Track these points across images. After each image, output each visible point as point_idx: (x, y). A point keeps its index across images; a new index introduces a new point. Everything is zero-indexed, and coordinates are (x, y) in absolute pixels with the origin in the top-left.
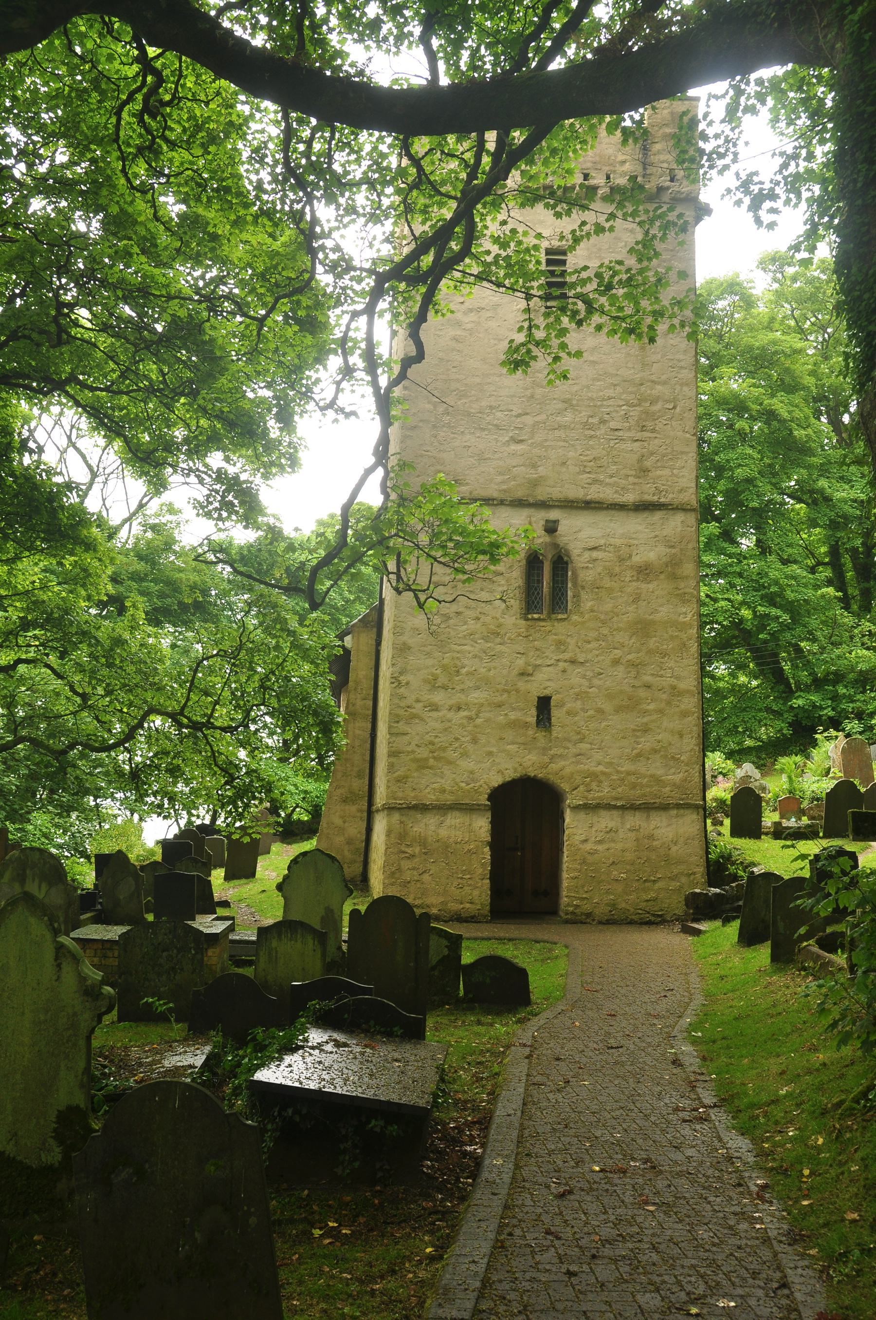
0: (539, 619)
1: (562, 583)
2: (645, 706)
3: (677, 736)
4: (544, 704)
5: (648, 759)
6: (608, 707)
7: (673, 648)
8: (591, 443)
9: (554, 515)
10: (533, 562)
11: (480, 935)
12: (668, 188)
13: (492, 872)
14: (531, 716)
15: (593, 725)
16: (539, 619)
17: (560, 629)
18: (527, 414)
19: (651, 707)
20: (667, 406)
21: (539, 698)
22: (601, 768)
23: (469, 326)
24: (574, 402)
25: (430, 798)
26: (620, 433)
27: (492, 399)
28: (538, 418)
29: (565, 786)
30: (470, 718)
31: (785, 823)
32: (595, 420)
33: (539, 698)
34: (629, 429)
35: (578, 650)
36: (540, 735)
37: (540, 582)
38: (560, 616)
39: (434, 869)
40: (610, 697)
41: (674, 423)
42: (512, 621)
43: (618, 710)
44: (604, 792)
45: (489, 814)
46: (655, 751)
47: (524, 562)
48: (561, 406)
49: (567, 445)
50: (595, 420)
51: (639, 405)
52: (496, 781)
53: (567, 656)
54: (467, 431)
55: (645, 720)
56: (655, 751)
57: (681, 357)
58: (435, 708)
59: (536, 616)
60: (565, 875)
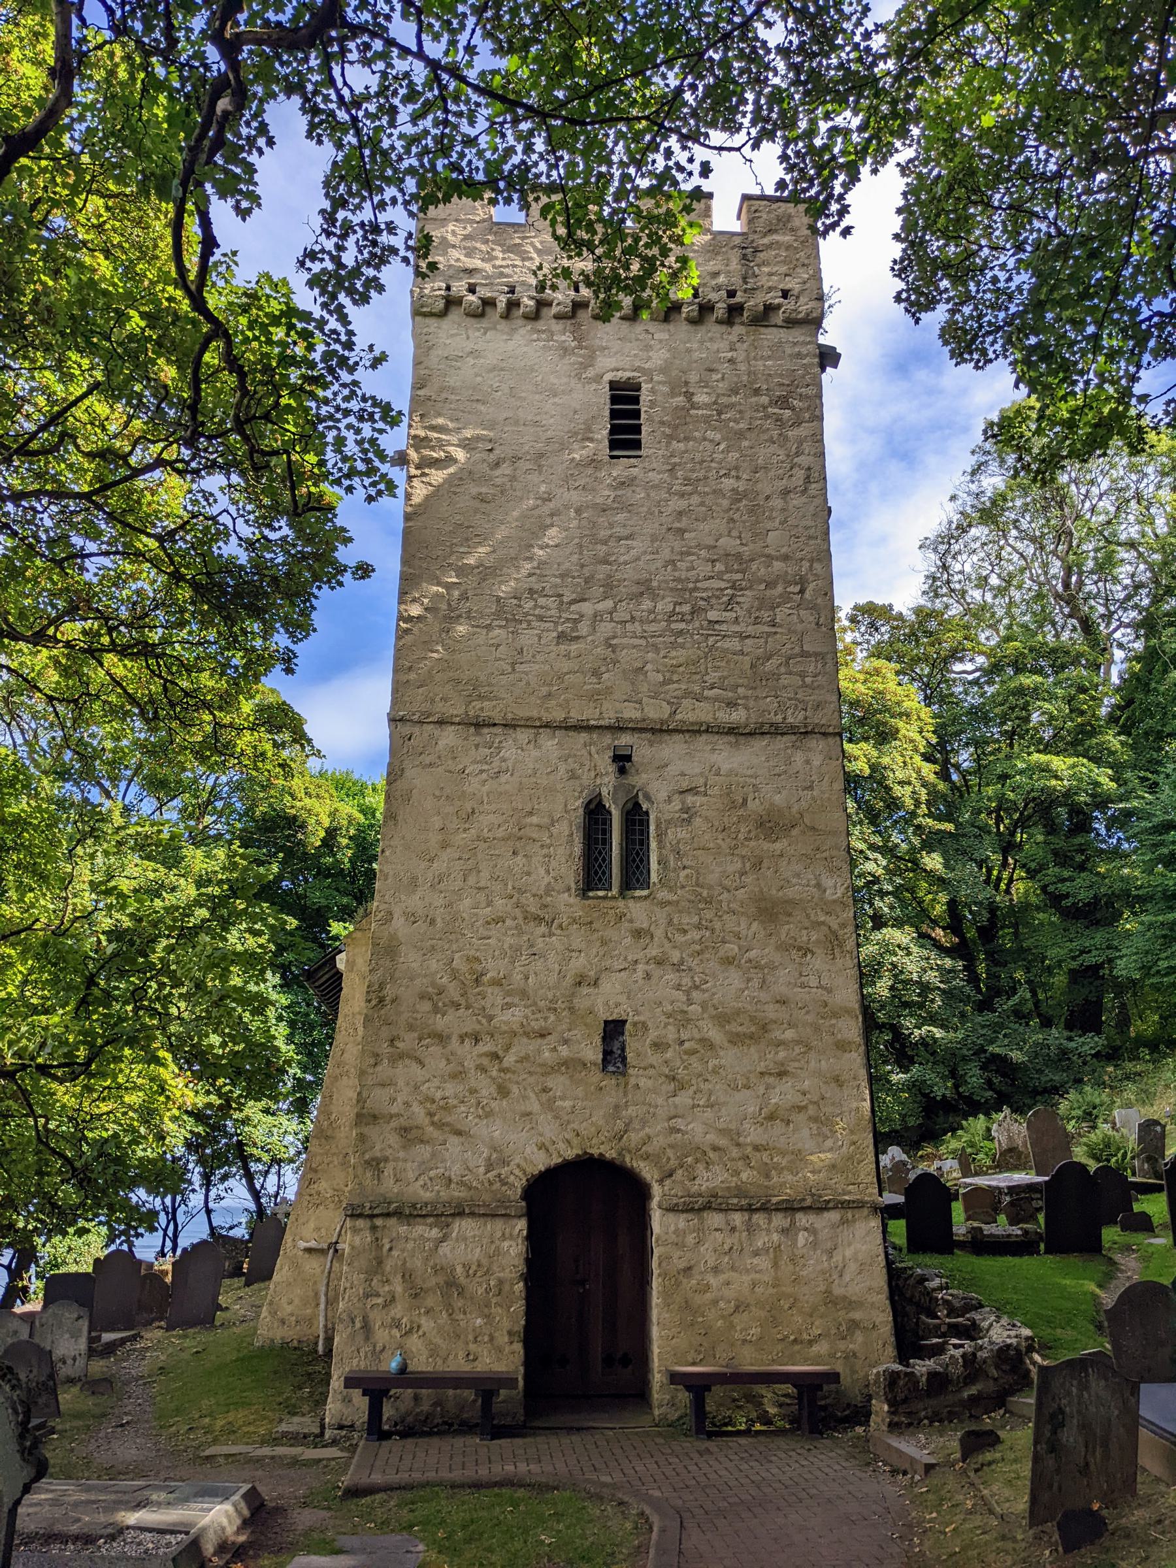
0: (605, 898)
1: (642, 843)
2: (777, 1034)
3: (833, 1085)
4: (613, 1030)
5: (788, 1122)
6: (715, 1034)
7: (818, 941)
8: (680, 640)
9: (625, 739)
10: (595, 813)
11: (483, 1472)
12: (779, 306)
13: (527, 1328)
14: (593, 1052)
15: (696, 1064)
16: (605, 898)
17: (637, 910)
18: (584, 600)
19: (790, 1034)
20: (791, 589)
21: (606, 1022)
22: (711, 1137)
23: (498, 481)
24: (655, 584)
25: (421, 1192)
26: (724, 627)
27: (533, 579)
28: (601, 606)
29: (647, 1172)
30: (495, 1056)
31: (988, 1229)
32: (686, 608)
33: (606, 1022)
34: (736, 621)
35: (667, 945)
36: (609, 1082)
37: (607, 842)
38: (638, 893)
39: (427, 1324)
40: (722, 1019)
41: (802, 612)
42: (568, 903)
43: (735, 1040)
44: (711, 1179)
45: (521, 1226)
46: (801, 1109)
47: (581, 811)
48: (635, 589)
49: (643, 642)
50: (686, 608)
51: (750, 588)
52: (541, 1162)
53: (653, 952)
54: (496, 623)
55: (782, 1054)
56: (801, 1109)
57: (810, 523)
58: (441, 1038)
59: (601, 893)
60: (655, 1332)
